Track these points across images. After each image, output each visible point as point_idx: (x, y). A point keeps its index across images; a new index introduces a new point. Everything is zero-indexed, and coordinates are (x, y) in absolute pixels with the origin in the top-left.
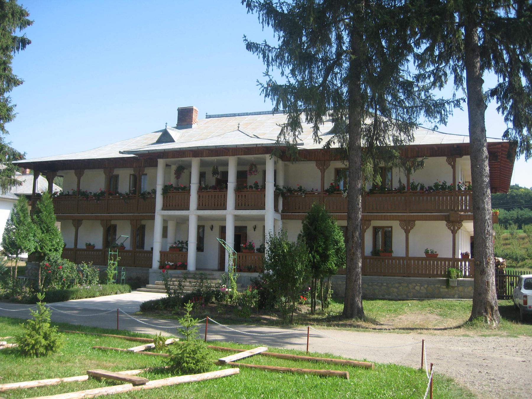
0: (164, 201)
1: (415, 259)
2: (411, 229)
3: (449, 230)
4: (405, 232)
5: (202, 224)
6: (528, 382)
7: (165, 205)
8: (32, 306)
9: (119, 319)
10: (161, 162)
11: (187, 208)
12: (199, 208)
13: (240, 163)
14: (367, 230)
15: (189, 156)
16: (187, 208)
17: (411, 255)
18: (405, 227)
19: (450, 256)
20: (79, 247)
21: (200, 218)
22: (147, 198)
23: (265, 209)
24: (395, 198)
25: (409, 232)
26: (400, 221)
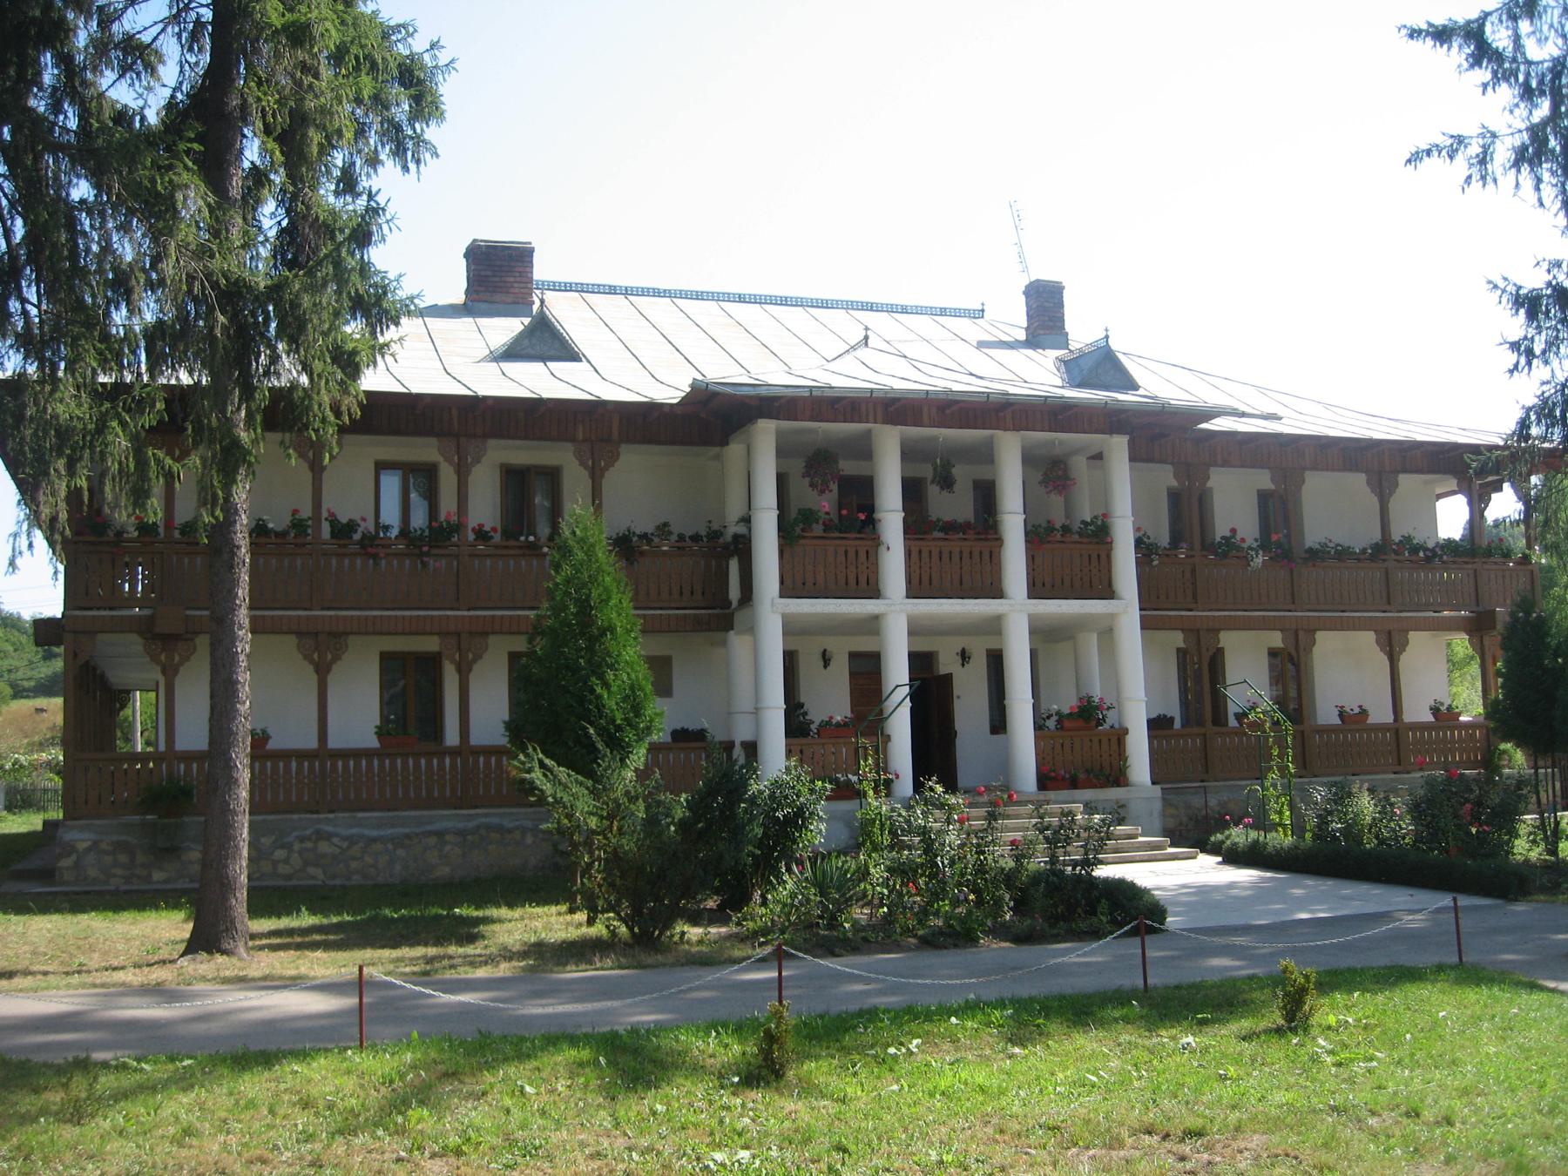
0: (1110, 571)
1: (345, 754)
2: (475, 660)
3: (306, 663)
4: (317, 672)
5: (924, 646)
6: (282, 1112)
7: (915, 581)
8: (1075, 949)
9: (1147, 960)
10: (766, 434)
11: (997, 592)
12: (911, 594)
13: (909, 453)
14: (334, 667)
15: (871, 419)
16: (997, 592)
17: (334, 743)
18: (316, 656)
19: (312, 743)
20: (1409, 716)
21: (792, 629)
22: (642, 553)
23: (1029, 597)
24: (347, 562)
25: (470, 670)
26: (300, 634)
